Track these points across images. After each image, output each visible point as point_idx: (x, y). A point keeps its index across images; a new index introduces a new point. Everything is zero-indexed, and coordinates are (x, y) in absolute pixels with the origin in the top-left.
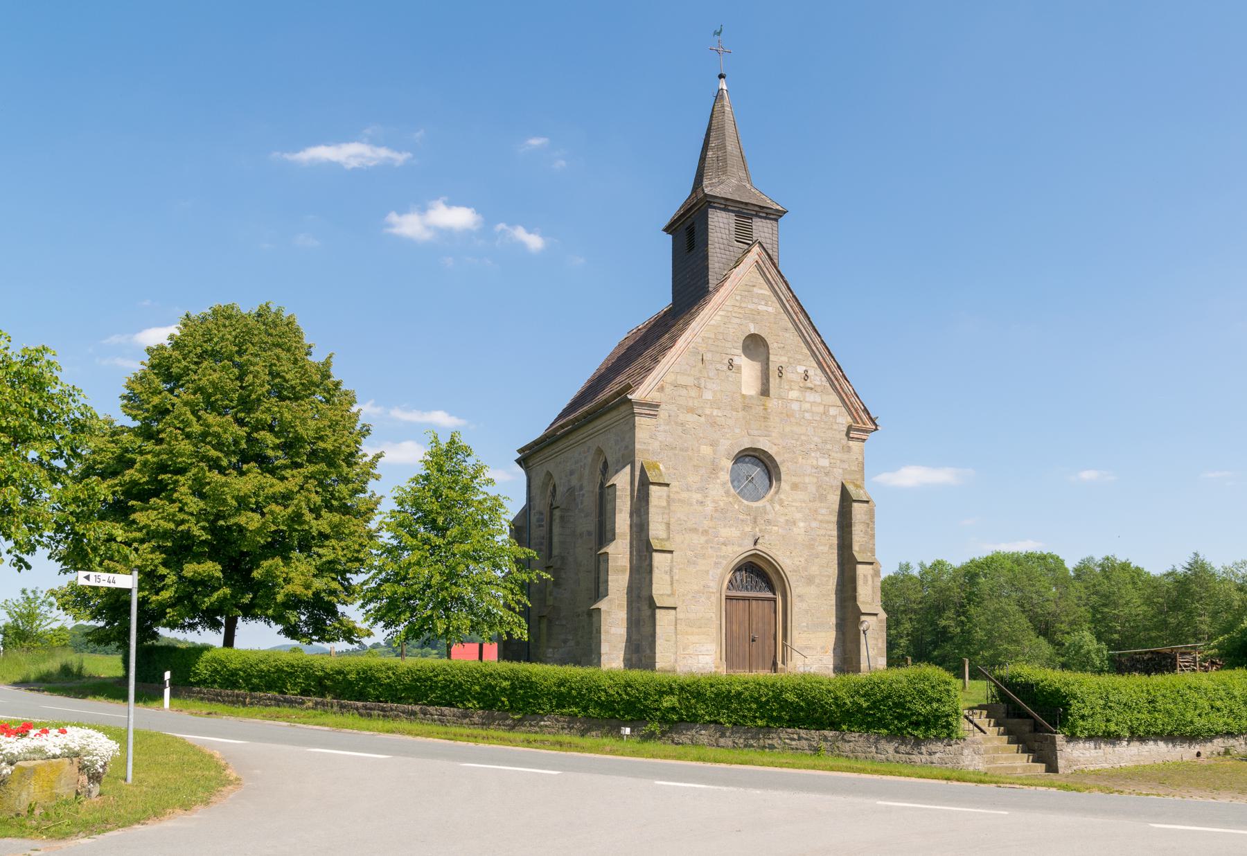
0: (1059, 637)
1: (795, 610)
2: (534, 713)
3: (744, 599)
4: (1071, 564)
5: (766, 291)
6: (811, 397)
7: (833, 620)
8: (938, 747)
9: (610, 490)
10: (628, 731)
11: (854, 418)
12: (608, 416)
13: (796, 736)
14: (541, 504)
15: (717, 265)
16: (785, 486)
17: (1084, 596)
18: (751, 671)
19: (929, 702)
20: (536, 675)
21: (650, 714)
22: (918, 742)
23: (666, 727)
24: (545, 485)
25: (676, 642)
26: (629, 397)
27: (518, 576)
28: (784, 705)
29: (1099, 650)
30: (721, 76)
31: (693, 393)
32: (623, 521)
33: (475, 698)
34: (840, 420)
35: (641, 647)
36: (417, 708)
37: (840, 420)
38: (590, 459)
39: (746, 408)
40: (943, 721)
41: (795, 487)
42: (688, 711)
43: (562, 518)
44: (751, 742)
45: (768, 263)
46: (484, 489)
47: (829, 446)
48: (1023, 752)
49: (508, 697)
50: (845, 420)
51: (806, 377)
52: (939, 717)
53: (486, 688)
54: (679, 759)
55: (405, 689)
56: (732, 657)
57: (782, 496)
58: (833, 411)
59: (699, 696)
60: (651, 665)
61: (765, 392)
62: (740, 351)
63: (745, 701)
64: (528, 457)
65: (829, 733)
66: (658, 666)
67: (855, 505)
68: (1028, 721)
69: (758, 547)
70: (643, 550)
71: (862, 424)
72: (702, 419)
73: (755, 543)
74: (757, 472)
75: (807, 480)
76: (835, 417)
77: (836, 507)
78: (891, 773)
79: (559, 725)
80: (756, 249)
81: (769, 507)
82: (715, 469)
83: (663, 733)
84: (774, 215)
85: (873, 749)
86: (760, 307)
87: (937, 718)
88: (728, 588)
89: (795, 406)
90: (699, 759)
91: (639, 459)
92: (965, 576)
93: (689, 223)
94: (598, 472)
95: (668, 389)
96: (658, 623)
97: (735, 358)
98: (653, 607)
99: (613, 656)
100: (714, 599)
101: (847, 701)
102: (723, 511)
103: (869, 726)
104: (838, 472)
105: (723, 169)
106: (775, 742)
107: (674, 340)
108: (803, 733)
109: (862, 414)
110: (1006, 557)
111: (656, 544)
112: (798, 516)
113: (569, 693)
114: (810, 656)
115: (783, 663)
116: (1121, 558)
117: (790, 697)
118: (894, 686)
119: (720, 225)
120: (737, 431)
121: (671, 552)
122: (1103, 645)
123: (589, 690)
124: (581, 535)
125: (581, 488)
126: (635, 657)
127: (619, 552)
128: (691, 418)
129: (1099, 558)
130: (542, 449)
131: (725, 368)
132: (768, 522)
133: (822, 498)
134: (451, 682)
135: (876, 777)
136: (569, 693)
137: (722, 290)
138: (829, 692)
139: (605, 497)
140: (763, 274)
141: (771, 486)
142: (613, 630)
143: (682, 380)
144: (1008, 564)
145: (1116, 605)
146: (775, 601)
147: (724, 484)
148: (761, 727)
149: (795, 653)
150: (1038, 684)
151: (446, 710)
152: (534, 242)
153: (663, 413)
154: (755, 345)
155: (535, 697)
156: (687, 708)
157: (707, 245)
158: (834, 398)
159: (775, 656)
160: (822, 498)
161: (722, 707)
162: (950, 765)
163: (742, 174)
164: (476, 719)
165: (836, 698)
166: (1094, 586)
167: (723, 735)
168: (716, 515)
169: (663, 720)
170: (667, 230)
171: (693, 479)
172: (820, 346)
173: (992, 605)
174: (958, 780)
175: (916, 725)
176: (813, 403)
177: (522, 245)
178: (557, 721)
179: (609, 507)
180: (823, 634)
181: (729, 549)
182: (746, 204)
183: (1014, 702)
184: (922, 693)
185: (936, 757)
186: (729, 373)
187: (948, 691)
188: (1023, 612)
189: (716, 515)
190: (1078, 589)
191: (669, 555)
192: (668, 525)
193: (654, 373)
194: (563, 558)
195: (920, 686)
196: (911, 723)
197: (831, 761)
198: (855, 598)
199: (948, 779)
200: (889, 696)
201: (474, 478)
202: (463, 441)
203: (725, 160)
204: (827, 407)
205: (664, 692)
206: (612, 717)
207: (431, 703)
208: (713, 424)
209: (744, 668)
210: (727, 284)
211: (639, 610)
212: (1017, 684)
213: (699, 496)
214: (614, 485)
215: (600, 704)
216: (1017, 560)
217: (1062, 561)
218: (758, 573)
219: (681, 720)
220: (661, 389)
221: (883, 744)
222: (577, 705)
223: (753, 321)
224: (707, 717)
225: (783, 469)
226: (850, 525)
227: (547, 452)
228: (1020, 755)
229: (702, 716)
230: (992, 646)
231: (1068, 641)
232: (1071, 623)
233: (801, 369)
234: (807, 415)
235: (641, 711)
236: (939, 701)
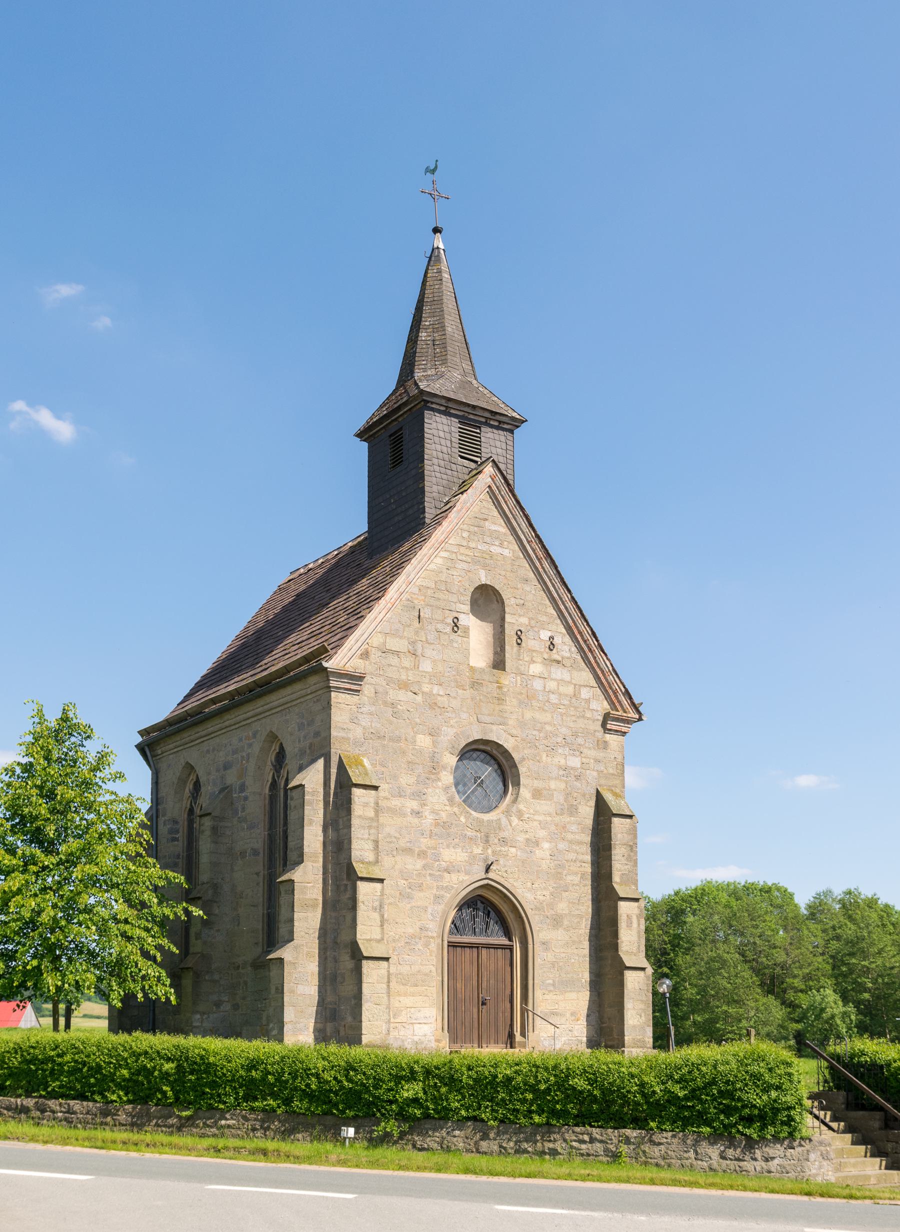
0: (790, 995)
1: (538, 961)
2: (211, 1108)
3: (471, 946)
4: (803, 899)
5: (503, 529)
6: (559, 673)
7: (586, 976)
8: (776, 1150)
9: (295, 794)
10: (351, 1132)
11: (611, 703)
12: (289, 690)
13: (586, 1138)
14: (175, 808)
15: (435, 488)
16: (525, 792)
17: (822, 943)
19: (766, 1090)
20: (216, 1054)
21: (358, 1106)
22: (751, 1144)
23: (405, 1127)
24: (182, 782)
25: (388, 1007)
26: (325, 664)
27: (156, 910)
28: (574, 1094)
29: (845, 1015)
30: (436, 230)
31: (407, 662)
32: (313, 837)
33: (121, 1088)
34: (594, 705)
35: (340, 1012)
36: (30, 1102)
37: (594, 705)
38: (256, 749)
39: (475, 684)
40: (783, 1116)
41: (537, 794)
42: (436, 1104)
43: (214, 829)
44: (525, 1145)
45: (504, 489)
46: (110, 786)
47: (580, 740)
48: (872, 1156)
49: (172, 1085)
50: (601, 706)
51: (552, 646)
52: (778, 1110)
53: (138, 1073)
54: (439, 1170)
55: (10, 1075)
56: (457, 1027)
57: (521, 807)
58: (585, 693)
59: (452, 1082)
60: (355, 1039)
61: (499, 663)
62: (467, 608)
63: (517, 1089)
64: (152, 744)
65: (632, 1133)
66: (365, 1039)
67: (615, 820)
68: (878, 1115)
69: (491, 875)
70: (343, 880)
71: (622, 710)
72: (419, 698)
73: (487, 870)
74: (487, 772)
75: (553, 784)
76: (588, 701)
77: (589, 822)
78: (731, 1187)
79: (249, 1125)
80: (489, 469)
81: (504, 821)
82: (435, 768)
83: (402, 1135)
84: (508, 424)
85: (692, 1154)
86: (493, 549)
87: (776, 1111)
88: (451, 933)
89: (538, 685)
90: (467, 1171)
91: (336, 750)
92: (668, 912)
93: (393, 428)
94: (269, 766)
95: (375, 655)
96: (365, 979)
97: (462, 617)
98: (357, 956)
99: (299, 1030)
100: (434, 946)
101: (657, 1089)
102: (446, 825)
103: (686, 1123)
104: (591, 775)
105: (441, 357)
106: (559, 1146)
107: (381, 589)
108: (596, 1133)
109: (622, 698)
110: (719, 888)
111: (622, 892)
112: (542, 834)
113: (264, 1079)
114: (557, 1028)
115: (523, 1034)
116: (866, 892)
117: (580, 1083)
118: (721, 1068)
119: (440, 433)
120: (464, 716)
121: (381, 881)
122: (851, 1008)
123: (294, 1075)
124: (243, 854)
125: (243, 788)
126: (329, 1027)
127: (308, 880)
128: (403, 696)
129: (838, 891)
130: (179, 731)
131: (448, 629)
132: (504, 841)
133: (572, 810)
134: (84, 1064)
135: (713, 1192)
136: (264, 1079)
137: (445, 523)
138: (632, 1076)
139: (282, 806)
140: (498, 506)
141: (505, 792)
142: (301, 989)
143: (394, 644)
144: (724, 898)
145: (865, 955)
146: (511, 950)
147: (446, 789)
148: (539, 1125)
149: (538, 1021)
150: (889, 1065)
151: (76, 1105)
152: (64, 430)
153: (367, 689)
154: (487, 600)
155: (214, 1085)
156: (435, 1100)
157: (422, 460)
158: (586, 676)
159: (512, 1026)
160: (572, 810)
161: (484, 1098)
162: (792, 1175)
163: (467, 366)
164: (122, 1117)
165: (642, 1085)
166: (834, 928)
167: (485, 1137)
168: (436, 830)
169: (402, 1116)
170: (361, 435)
171: (407, 780)
172: (569, 604)
173: (706, 952)
174: (822, 1195)
175: (749, 1121)
176: (560, 682)
177: (43, 435)
178: (246, 1119)
179: (292, 816)
180: (573, 995)
181: (454, 877)
182: (474, 407)
183: (857, 1088)
184: (756, 1077)
185: (773, 1165)
186: (454, 636)
187: (790, 1075)
188: (746, 961)
189: (436, 830)
190: (813, 935)
191: (378, 886)
192: (376, 842)
193: (357, 633)
194: (215, 887)
195: (754, 1068)
196: (742, 1118)
197: (638, 1172)
198: (615, 947)
199: (809, 1194)
200: (713, 1082)
201: (95, 769)
202: (81, 717)
203: (444, 346)
204: (578, 687)
205: (402, 1078)
206: (325, 1113)
207: (53, 1095)
208: (433, 706)
209: (471, 1041)
210: (453, 515)
211: (336, 961)
212: (860, 1065)
213: (414, 804)
214: (301, 786)
215: (309, 1095)
216: (736, 893)
217: (791, 896)
218: (489, 911)
219: (427, 1116)
220: (365, 655)
221: (705, 1148)
222: (275, 1096)
223: (484, 566)
224: (463, 1113)
225: (522, 770)
226: (608, 848)
227: (187, 736)
228: (870, 1160)
229: (456, 1111)
230: (707, 1007)
231: (804, 1001)
232: (808, 978)
233: (545, 635)
234: (554, 698)
235: (369, 1104)
236: (778, 1088)
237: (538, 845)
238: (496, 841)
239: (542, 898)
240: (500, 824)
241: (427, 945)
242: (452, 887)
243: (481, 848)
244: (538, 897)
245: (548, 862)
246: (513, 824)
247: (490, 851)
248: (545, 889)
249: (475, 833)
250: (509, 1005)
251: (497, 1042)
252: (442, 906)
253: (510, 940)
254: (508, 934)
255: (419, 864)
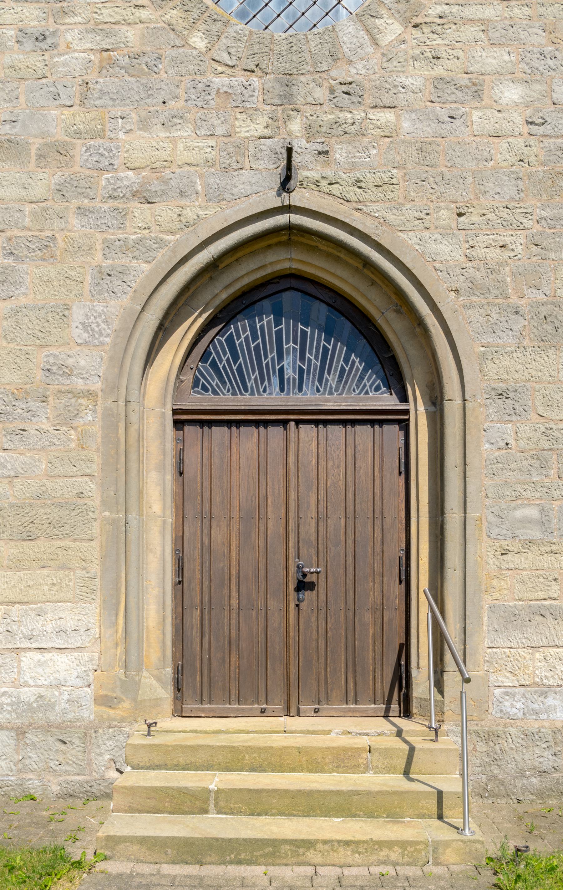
1: (483, 450)
18: (258, 704)
112: (492, 59)
146: (404, 425)
159: (405, 648)
181: (165, 212)
237: (478, 95)
238: (321, 94)
239: (495, 254)
240: (335, 43)
241: (68, 418)
242: (161, 243)
243: (263, 120)
244: (480, 252)
245: (519, 143)
246: (386, 39)
247: (296, 126)
248: (507, 226)
249: (241, 78)
250: (397, 590)
251: (352, 696)
252: (125, 300)
253: (404, 399)
254: (395, 380)
255: (44, 182)
